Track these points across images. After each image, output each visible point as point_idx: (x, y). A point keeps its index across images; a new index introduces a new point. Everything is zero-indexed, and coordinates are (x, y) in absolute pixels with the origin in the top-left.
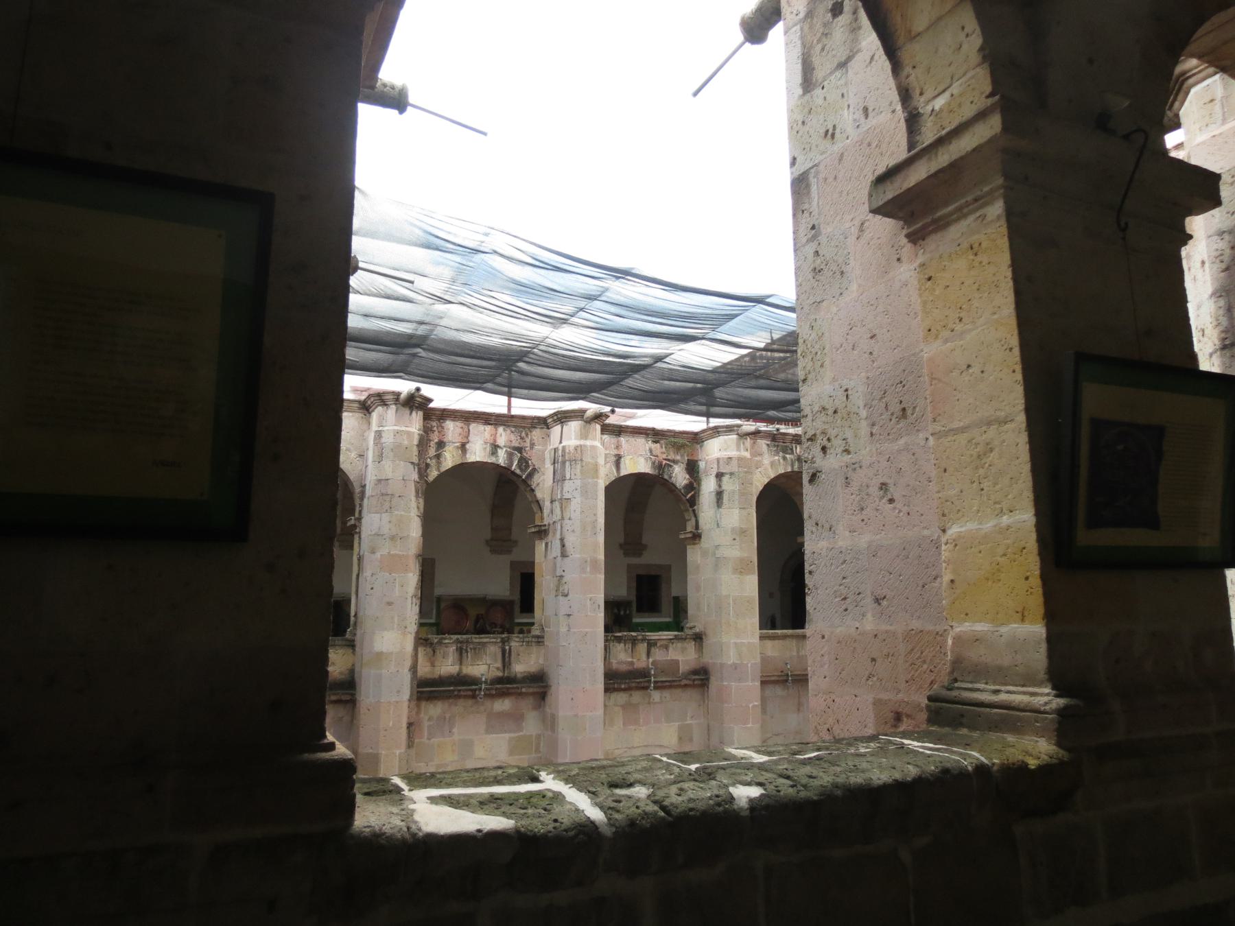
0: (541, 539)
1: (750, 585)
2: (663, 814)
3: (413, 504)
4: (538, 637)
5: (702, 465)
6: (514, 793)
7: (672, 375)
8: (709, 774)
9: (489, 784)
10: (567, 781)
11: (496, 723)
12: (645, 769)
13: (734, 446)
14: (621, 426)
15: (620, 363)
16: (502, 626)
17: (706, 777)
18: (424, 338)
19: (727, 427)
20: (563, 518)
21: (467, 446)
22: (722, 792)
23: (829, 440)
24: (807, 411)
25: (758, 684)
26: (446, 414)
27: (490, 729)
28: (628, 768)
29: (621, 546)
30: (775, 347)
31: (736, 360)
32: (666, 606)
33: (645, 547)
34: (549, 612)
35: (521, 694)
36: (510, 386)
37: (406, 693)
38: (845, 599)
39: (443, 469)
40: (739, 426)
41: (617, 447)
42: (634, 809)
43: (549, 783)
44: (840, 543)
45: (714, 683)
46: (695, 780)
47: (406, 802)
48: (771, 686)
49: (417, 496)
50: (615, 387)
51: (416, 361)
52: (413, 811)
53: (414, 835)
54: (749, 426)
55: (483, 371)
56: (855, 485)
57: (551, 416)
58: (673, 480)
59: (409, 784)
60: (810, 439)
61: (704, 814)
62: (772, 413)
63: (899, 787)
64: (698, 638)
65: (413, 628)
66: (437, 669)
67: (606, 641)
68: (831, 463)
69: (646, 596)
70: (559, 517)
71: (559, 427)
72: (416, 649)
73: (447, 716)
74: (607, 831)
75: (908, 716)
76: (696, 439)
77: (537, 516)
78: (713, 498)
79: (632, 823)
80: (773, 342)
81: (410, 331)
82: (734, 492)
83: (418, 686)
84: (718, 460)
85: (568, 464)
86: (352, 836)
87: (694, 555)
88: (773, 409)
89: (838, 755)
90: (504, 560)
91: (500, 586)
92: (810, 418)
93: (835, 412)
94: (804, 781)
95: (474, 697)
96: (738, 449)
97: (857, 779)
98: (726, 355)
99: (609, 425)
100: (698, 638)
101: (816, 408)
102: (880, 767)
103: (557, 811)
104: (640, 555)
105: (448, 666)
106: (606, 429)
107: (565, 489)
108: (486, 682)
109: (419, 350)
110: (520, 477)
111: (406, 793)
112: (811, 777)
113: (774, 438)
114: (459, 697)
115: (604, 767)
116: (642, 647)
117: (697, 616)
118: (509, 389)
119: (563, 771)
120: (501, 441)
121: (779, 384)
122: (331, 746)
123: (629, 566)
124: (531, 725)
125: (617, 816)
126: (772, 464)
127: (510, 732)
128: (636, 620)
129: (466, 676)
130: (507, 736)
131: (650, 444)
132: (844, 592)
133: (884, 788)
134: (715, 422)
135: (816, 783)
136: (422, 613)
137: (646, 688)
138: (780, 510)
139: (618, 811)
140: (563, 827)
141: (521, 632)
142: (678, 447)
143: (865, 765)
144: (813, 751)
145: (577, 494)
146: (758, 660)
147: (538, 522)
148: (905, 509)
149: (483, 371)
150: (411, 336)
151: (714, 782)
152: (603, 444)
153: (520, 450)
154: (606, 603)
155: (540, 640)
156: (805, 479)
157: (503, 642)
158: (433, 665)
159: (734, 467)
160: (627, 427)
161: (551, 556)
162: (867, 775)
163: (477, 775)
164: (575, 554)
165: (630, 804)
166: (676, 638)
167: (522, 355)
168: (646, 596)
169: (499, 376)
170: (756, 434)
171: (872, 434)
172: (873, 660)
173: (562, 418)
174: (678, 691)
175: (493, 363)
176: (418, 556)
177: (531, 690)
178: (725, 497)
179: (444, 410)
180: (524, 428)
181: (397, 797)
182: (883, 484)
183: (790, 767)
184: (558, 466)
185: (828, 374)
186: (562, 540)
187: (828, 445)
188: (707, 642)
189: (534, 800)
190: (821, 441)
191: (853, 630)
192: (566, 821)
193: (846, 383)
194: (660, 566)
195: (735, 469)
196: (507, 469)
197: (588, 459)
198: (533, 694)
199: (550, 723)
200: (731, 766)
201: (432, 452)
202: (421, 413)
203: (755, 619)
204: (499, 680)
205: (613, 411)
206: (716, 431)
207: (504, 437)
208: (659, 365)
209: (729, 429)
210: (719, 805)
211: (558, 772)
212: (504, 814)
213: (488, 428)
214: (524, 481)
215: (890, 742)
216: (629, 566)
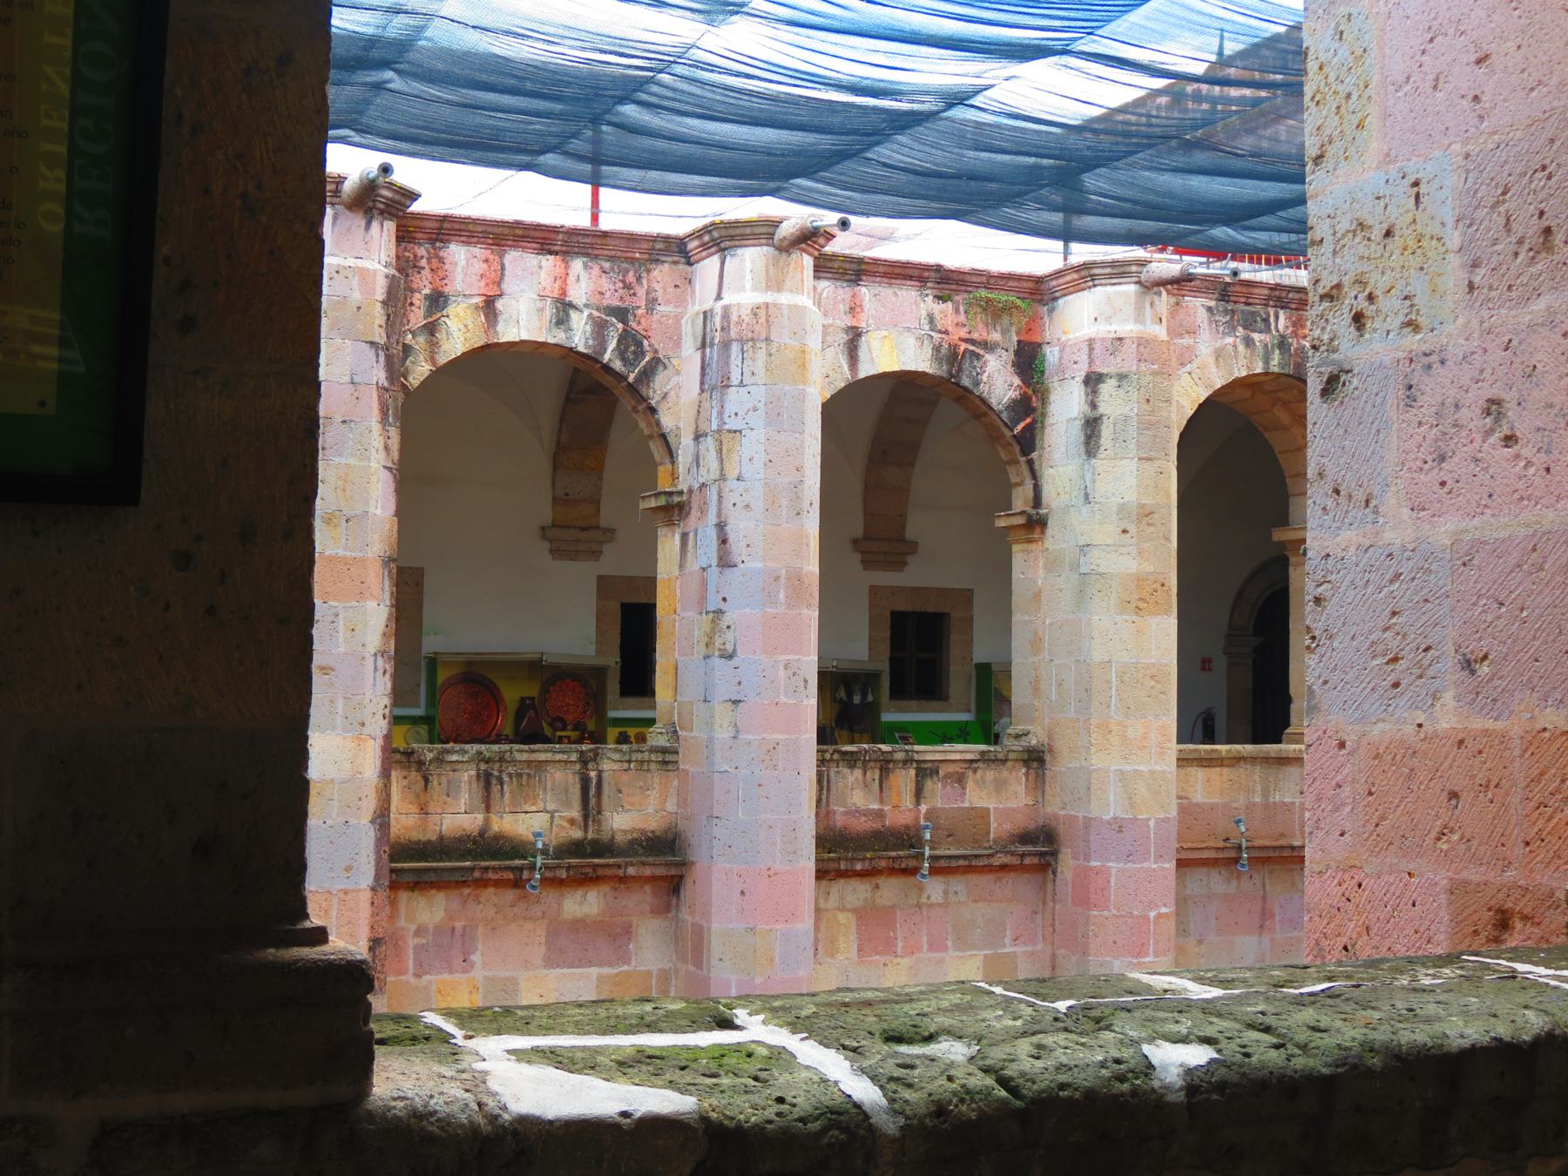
0: (671, 524)
1: (1158, 640)
2: (1003, 1093)
3: (377, 440)
4: (664, 751)
5: (1051, 355)
6: (688, 1048)
7: (982, 137)
8: (1098, 1021)
9: (630, 1030)
10: (795, 1026)
11: (569, 945)
12: (957, 1008)
13: (1129, 310)
14: (860, 261)
15: (1016, 129)
16: (578, 727)
17: (1090, 1026)
18: (403, 46)
19: (1113, 264)
20: (723, 476)
21: (499, 304)
22: (1126, 1054)
23: (1371, 298)
24: (1321, 229)
25: (1171, 865)
26: (448, 229)
28: (924, 1006)
29: (855, 542)
30: (1232, 72)
31: (1138, 103)
32: (959, 682)
33: (913, 547)
34: (691, 691)
35: (623, 880)
36: (597, 160)
37: (366, 874)
38: (1395, 660)
39: (443, 359)
40: (1142, 263)
41: (852, 310)
42: (943, 1081)
43: (756, 1029)
44: (1389, 535)
45: (1067, 863)
46: (1066, 1030)
47: (468, 1058)
48: (1201, 872)
49: (384, 420)
50: (850, 164)
51: (382, 100)
52: (486, 1073)
53: (493, 1119)
54: (1166, 264)
55: (539, 125)
56: (1428, 402)
57: (697, 234)
58: (983, 389)
59: (461, 1026)
60: (1328, 297)
61: (1090, 1095)
62: (1221, 232)
63: (1503, 1054)
64: (1035, 759)
65: (379, 726)
66: (433, 818)
67: (822, 762)
68: (1375, 352)
69: (913, 664)
70: (714, 474)
71: (714, 261)
72: (385, 774)
73: (459, 925)
74: (889, 1125)
75: (1525, 918)
76: (1039, 292)
77: (663, 471)
78: (1076, 433)
79: (940, 1110)
80: (1223, 61)
81: (370, 31)
82: (1127, 418)
83: (392, 859)
84: (1091, 343)
85: (735, 348)
86: (369, 1113)
87: (1027, 567)
88: (1229, 221)
89: (1375, 989)
90: (580, 577)
91: (574, 634)
92: (1327, 247)
93: (1388, 234)
94: (1302, 1036)
95: (518, 884)
96: (1139, 318)
97: (1414, 1035)
98: (1112, 92)
99: (834, 256)
100: (1035, 759)
101: (1344, 224)
102: (1465, 1012)
103: (782, 1081)
104: (900, 565)
105: (458, 815)
106: (827, 267)
107: (730, 408)
108: (544, 852)
109: (389, 74)
110: (621, 377)
111: (460, 1041)
112: (1315, 1029)
113: (1226, 292)
114: (482, 883)
115: (869, 1004)
116: (904, 779)
117: (1035, 707)
118: (595, 168)
119: (783, 1008)
120: (579, 292)
121: (1239, 164)
122: (320, 936)
123: (874, 590)
125: (907, 1094)
126: (1219, 354)
127: (600, 965)
128: (888, 717)
129: (499, 837)
130: (594, 971)
131: (929, 304)
132: (1394, 644)
133: (1473, 1053)
134: (1082, 252)
135: (1328, 1041)
136: (399, 695)
137: (913, 871)
138: (1240, 468)
139: (910, 1086)
140: (797, 1113)
141: (623, 739)
142: (995, 313)
143: (1431, 1009)
144: (1320, 980)
145: (757, 420)
146: (1173, 812)
147: (664, 485)
148: (1540, 460)
149: (539, 125)
150: (372, 42)
151: (1107, 1035)
152: (818, 302)
153: (622, 314)
154: (823, 675)
155: (667, 758)
156: (1314, 386)
157: (584, 761)
158: (423, 810)
159: (1126, 361)
160: (876, 262)
161: (693, 565)
162: (1438, 1028)
163: (602, 1013)
164: (752, 555)
165: (935, 1071)
166: (984, 758)
167: (630, 89)
168: (913, 664)
169: (575, 135)
170: (1182, 283)
171: (1471, 287)
172: (1454, 795)
173: (723, 238)
174: (985, 880)
175: (559, 107)
176: (388, 561)
177: (648, 871)
178: (1106, 431)
179: (445, 218)
180: (633, 260)
181: (444, 1049)
182: (1492, 401)
183: (1270, 1009)
184: (713, 353)
185: (1374, 143)
186: (721, 527)
187: (1370, 310)
188: (1062, 765)
189: (730, 1061)
190: (1352, 300)
191: (1410, 729)
192: (803, 1103)
193: (1414, 169)
194: (943, 592)
195: (1130, 366)
196: (591, 360)
197: (782, 336)
198: (653, 879)
200: (1144, 1005)
201: (417, 317)
202: (390, 226)
203: (1168, 719)
204: (575, 848)
205: (844, 224)
206: (1086, 275)
207: (585, 282)
208: (959, 113)
209: (1119, 271)
210: (1121, 1078)
211: (774, 1010)
212: (672, 1085)
213: (549, 262)
214: (633, 389)
215: (1486, 967)
216: (874, 590)
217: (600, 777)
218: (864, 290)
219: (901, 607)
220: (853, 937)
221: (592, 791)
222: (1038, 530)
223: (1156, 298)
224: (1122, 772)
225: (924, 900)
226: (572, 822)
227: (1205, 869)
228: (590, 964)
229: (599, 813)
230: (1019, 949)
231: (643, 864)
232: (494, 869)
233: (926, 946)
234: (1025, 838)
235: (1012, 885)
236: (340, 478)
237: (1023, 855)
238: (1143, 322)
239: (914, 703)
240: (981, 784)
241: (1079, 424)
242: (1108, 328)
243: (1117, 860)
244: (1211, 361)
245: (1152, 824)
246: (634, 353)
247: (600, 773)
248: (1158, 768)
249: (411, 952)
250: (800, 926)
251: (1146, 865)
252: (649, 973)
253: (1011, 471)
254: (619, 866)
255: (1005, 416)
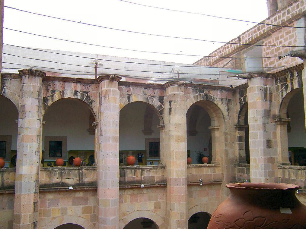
21: (65, 92)
27: (74, 204)
29: (143, 131)
39: (54, 101)
78: (168, 110)
85: (103, 98)
100: (163, 168)
104: (151, 134)
105: (56, 179)
116: (139, 172)
123: (146, 139)
124: (91, 202)
126: (194, 97)
127: (82, 205)
130: (81, 206)
153: (87, 93)
174: (155, 189)
177: (90, 189)
178: (172, 110)
188: (168, 168)
199: (98, 201)
207: (79, 87)
216: (146, 139)
217: (82, 173)
218: (131, 88)
219: (151, 141)
220: (130, 199)
221: (81, 175)
222: (163, 128)
223: (181, 88)
224: (176, 170)
225: (143, 192)
226: (77, 180)
227: (195, 186)
228: (81, 205)
229: (82, 178)
230: (161, 201)
231: (90, 187)
232: (62, 188)
233: (143, 201)
234: (162, 181)
235: (158, 190)
236: (28, 121)
237: (161, 184)
238: (179, 92)
239: (153, 157)
240: (153, 172)
241: (169, 109)
242: (173, 93)
243: (176, 186)
244: (193, 98)
245: (182, 179)
246: (89, 99)
247: (82, 171)
248: (183, 169)
249: (47, 204)
250: (253, 157)
251: (181, 186)
252: (92, 206)
253: (160, 118)
254: (85, 188)
255: (157, 109)
